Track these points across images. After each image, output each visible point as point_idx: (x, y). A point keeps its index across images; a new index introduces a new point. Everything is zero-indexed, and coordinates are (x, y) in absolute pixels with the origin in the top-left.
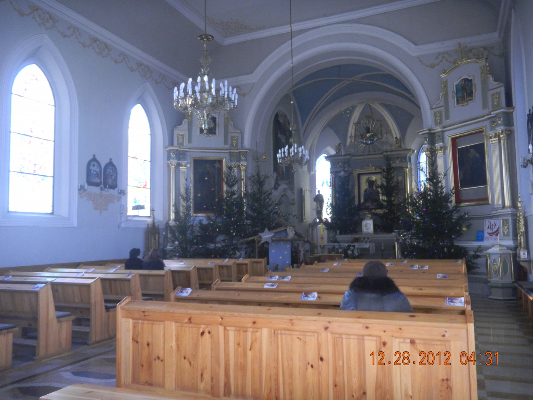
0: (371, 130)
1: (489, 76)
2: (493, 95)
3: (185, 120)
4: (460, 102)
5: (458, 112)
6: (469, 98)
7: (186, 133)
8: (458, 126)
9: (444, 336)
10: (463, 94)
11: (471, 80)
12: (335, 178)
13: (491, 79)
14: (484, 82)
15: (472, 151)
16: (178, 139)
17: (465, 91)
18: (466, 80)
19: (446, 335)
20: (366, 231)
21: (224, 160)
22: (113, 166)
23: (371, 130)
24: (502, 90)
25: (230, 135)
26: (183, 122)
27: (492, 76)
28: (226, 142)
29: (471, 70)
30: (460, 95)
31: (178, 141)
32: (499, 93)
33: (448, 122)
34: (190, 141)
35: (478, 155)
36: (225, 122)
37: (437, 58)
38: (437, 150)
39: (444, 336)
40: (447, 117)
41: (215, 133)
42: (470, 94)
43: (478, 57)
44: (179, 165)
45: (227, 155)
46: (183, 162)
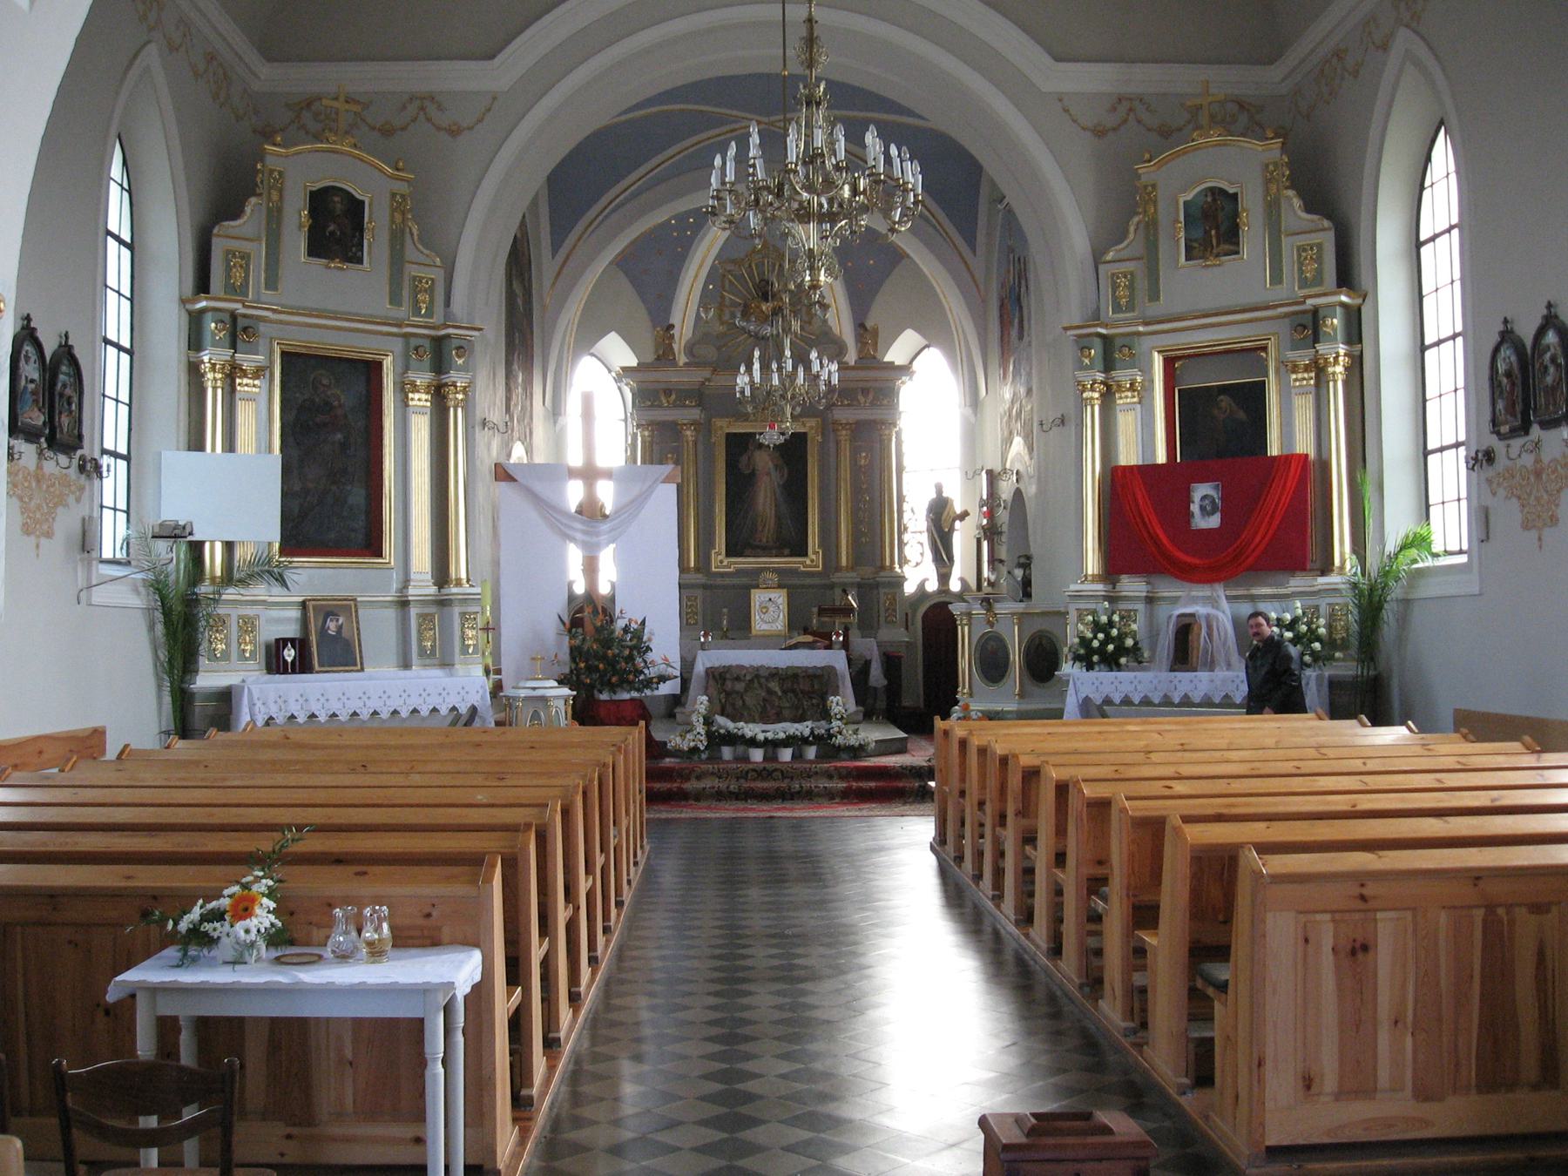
0: (758, 293)
1: (1291, 193)
2: (1301, 249)
3: (253, 200)
4: (1195, 253)
5: (1191, 284)
6: (1227, 247)
7: (259, 252)
8: (1196, 322)
9: (429, 915)
10: (1207, 233)
11: (1234, 197)
12: (651, 443)
13: (1297, 202)
14: (1273, 209)
15: (1225, 401)
16: (228, 269)
17: (1215, 226)
18: (1217, 192)
19: (434, 914)
20: (765, 627)
21: (388, 363)
22: (74, 362)
23: (758, 293)
24: (1328, 240)
25: (412, 270)
26: (248, 209)
27: (1300, 195)
28: (395, 299)
29: (1243, 166)
30: (1198, 234)
31: (228, 277)
32: (1320, 246)
33: (1153, 310)
34: (272, 283)
35: (1242, 415)
36: (393, 221)
37: (1114, 109)
38: (1120, 388)
39: (429, 915)
40: (1154, 295)
41: (360, 261)
42: (1230, 237)
43: (1255, 129)
44: (232, 373)
45: (398, 345)
46: (247, 361)
